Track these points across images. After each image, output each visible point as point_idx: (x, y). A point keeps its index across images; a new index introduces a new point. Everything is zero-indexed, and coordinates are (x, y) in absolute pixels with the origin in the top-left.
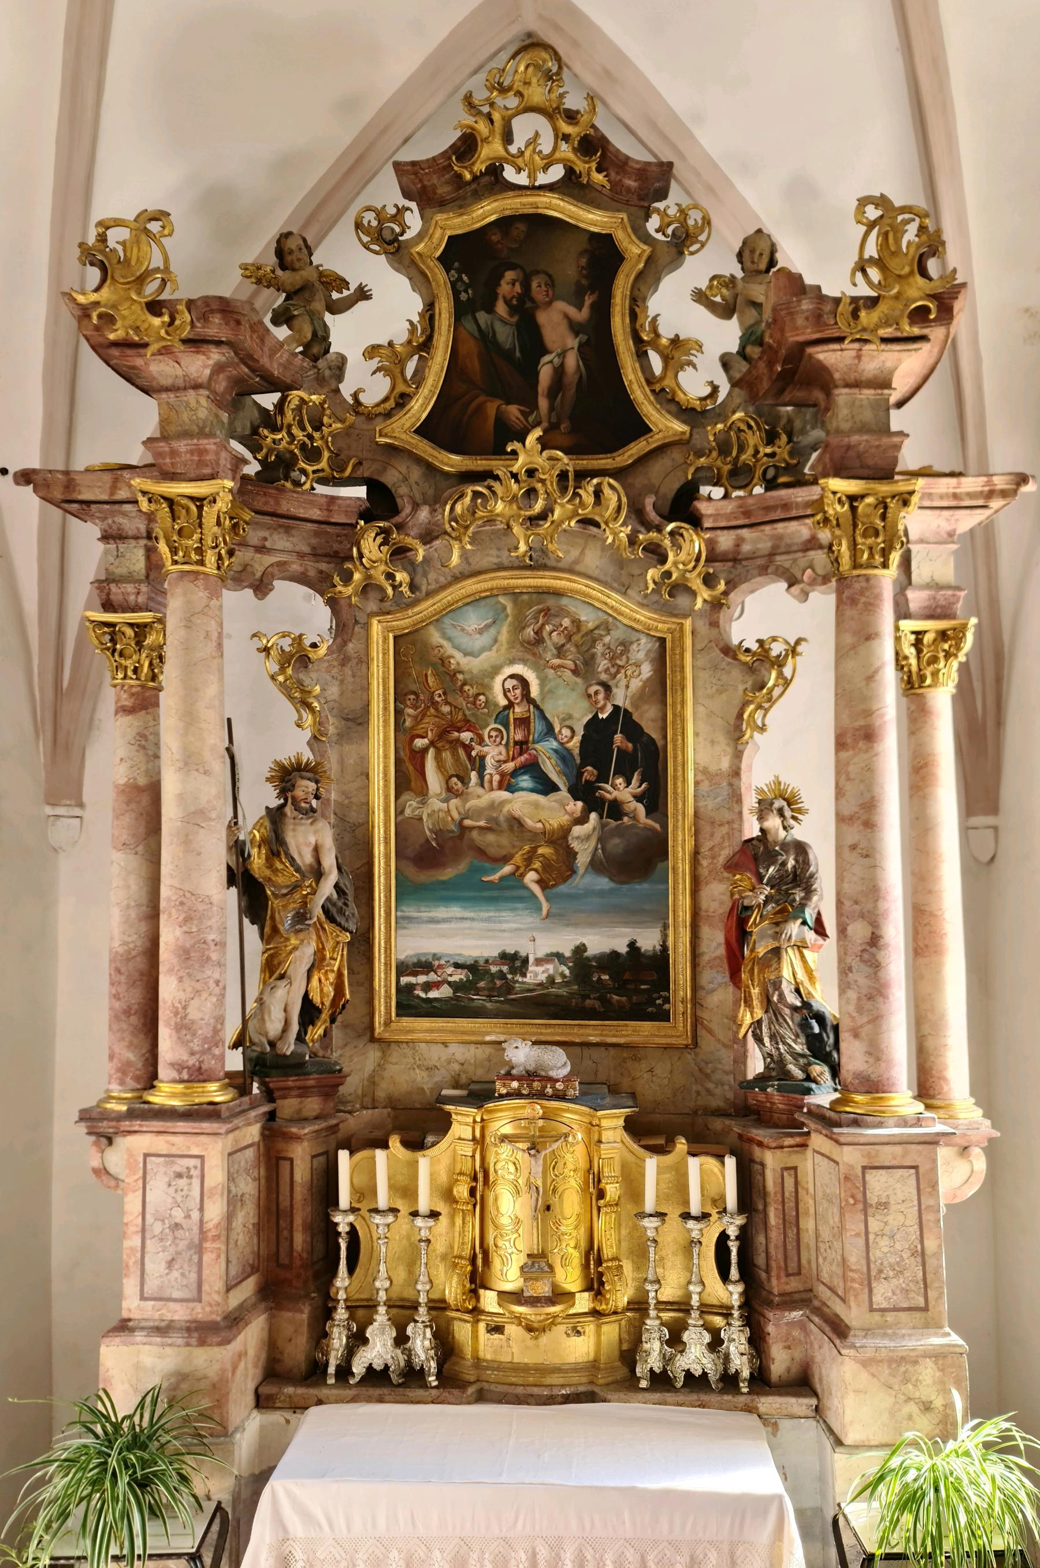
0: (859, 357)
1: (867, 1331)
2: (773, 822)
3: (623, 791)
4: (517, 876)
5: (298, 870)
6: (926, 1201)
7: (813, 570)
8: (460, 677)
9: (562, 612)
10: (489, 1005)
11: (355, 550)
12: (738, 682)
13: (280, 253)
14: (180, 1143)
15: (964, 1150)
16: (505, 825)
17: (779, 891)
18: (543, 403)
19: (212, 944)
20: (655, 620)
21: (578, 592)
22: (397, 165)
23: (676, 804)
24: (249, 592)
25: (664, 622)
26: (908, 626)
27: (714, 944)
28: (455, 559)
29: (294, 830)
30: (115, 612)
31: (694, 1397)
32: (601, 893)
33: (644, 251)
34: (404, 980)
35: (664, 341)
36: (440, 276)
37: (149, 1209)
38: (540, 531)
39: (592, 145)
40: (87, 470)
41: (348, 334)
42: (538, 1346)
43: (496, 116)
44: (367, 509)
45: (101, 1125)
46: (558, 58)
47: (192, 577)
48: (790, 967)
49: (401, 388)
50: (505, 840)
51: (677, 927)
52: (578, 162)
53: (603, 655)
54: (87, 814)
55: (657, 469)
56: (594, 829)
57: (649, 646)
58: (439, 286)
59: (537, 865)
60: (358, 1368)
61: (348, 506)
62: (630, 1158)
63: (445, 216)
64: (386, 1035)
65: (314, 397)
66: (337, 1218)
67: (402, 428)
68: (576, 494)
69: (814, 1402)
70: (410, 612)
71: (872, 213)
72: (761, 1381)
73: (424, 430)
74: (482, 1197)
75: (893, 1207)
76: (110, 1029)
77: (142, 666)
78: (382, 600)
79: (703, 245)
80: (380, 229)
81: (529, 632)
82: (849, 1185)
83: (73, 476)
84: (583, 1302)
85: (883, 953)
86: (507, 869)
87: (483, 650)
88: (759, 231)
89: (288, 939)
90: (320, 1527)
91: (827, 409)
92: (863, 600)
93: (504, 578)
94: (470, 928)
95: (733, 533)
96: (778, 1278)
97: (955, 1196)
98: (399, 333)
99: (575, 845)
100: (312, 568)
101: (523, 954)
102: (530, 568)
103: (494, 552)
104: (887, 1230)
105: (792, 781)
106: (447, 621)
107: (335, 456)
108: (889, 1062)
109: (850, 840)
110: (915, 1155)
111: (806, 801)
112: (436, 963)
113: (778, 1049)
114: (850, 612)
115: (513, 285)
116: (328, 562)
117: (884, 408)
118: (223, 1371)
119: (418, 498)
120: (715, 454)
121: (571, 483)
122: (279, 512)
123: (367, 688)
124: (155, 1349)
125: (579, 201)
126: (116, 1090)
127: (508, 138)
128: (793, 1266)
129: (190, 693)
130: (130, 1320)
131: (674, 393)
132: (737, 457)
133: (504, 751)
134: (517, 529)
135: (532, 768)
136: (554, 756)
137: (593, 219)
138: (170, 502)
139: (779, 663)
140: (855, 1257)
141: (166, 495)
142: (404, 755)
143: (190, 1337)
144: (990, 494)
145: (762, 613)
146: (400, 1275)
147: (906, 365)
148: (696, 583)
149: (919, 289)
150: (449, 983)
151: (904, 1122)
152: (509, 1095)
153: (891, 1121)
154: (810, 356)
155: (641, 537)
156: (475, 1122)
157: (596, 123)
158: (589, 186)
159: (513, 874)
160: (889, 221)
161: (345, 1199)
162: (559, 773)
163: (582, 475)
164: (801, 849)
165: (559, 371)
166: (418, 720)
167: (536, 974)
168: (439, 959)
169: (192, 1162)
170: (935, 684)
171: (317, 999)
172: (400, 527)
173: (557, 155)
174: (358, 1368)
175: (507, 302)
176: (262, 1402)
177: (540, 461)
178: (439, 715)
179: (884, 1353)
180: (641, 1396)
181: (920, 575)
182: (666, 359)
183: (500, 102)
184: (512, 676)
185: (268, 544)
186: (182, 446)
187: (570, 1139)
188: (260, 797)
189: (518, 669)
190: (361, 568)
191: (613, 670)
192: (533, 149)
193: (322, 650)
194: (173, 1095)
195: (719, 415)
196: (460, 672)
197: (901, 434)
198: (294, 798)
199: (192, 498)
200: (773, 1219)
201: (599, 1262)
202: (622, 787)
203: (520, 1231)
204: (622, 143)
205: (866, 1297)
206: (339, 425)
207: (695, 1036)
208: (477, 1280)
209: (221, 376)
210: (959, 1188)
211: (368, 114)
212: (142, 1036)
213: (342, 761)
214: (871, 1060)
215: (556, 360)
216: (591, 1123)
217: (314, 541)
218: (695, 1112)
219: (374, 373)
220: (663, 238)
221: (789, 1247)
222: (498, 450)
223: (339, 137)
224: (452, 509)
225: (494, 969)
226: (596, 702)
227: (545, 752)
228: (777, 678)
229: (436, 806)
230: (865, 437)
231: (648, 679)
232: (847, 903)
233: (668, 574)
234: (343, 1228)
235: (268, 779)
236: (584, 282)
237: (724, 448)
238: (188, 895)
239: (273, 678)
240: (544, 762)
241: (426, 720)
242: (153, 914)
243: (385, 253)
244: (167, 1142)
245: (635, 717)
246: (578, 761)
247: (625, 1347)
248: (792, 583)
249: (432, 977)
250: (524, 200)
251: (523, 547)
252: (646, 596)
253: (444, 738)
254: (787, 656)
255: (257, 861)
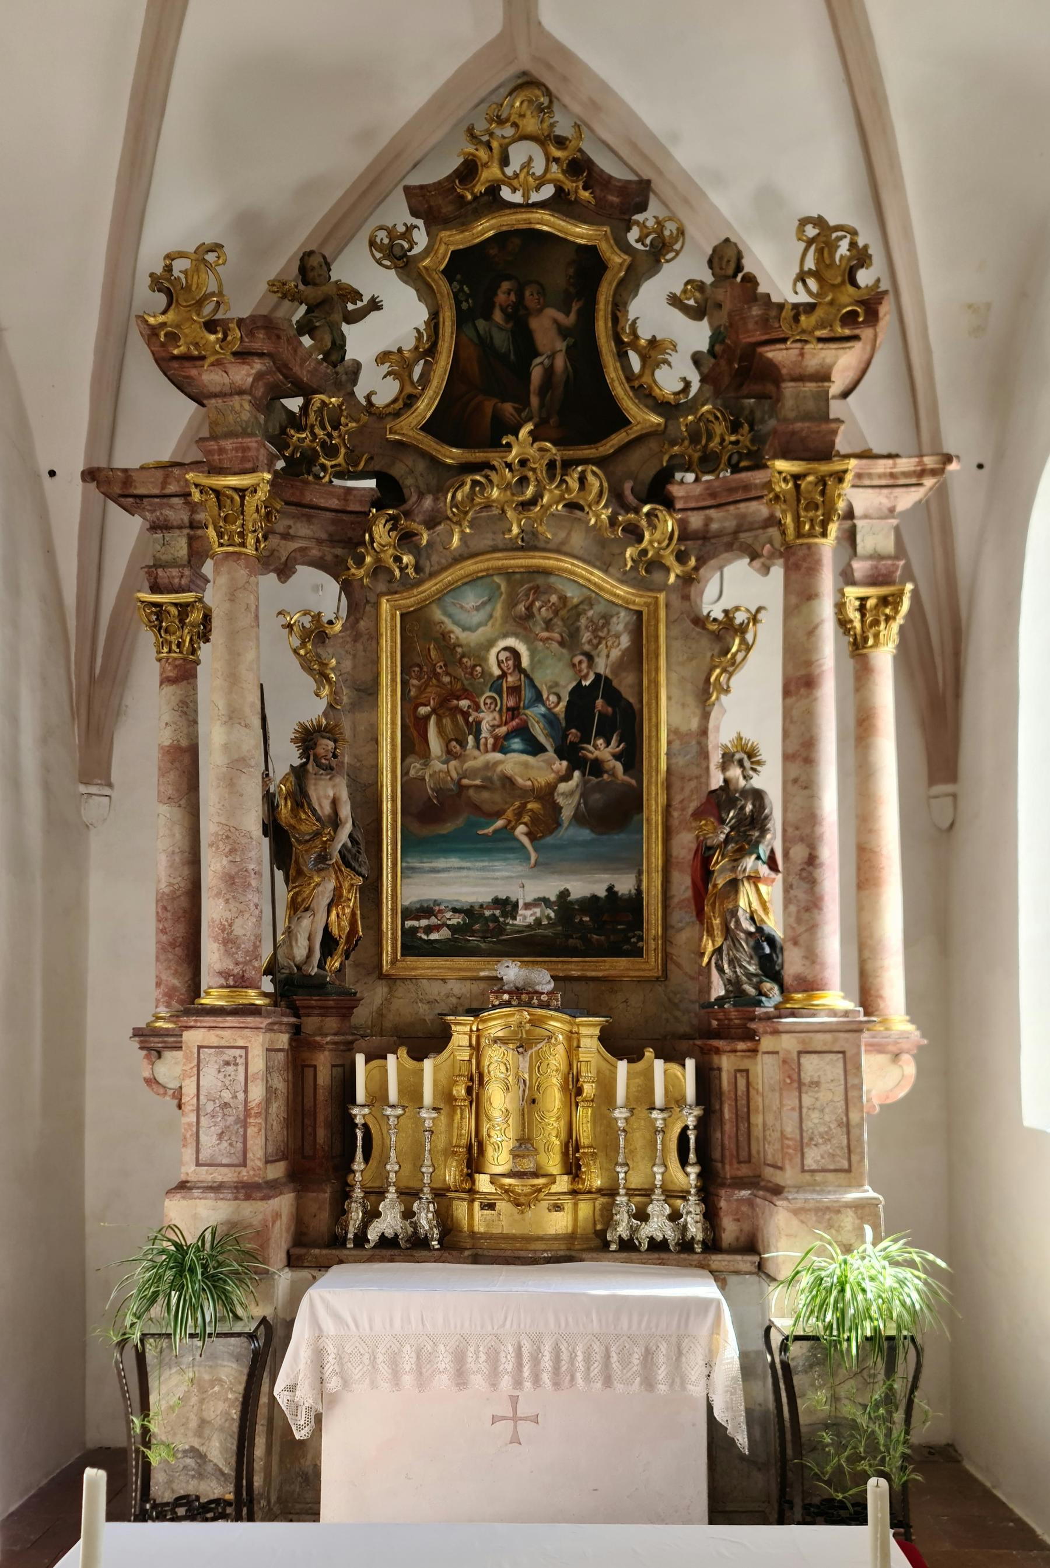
0: (802, 355)
1: (799, 1188)
2: (735, 772)
3: (602, 750)
4: (508, 830)
5: (319, 819)
6: (852, 1081)
7: (772, 545)
8: (459, 650)
9: (550, 589)
10: (483, 945)
11: (367, 535)
12: (706, 647)
13: (303, 270)
14: (227, 1037)
15: (896, 1056)
16: (498, 783)
17: (738, 832)
18: (534, 401)
19: (252, 873)
20: (633, 594)
21: (565, 570)
22: (407, 190)
23: (650, 762)
24: (273, 576)
25: (641, 596)
26: (852, 593)
27: (683, 887)
28: (456, 541)
29: (315, 784)
30: (161, 593)
31: (656, 1255)
32: (585, 844)
33: (625, 260)
34: (409, 924)
35: (643, 342)
36: (443, 287)
37: (203, 1092)
38: (531, 514)
39: (580, 167)
40: (142, 468)
41: (362, 342)
42: (524, 1220)
43: (495, 144)
44: (379, 499)
45: (153, 1042)
46: (548, 93)
47: (235, 558)
48: (746, 898)
49: (409, 389)
50: (497, 797)
51: (648, 877)
52: (567, 182)
53: (587, 627)
54: (114, 794)
55: (637, 456)
56: (577, 786)
57: (627, 619)
58: (443, 296)
59: (526, 819)
60: (373, 1235)
61: (362, 496)
62: (605, 1065)
63: (448, 233)
64: (393, 972)
65: (333, 400)
66: (355, 1111)
67: (408, 427)
68: (563, 481)
69: (756, 1259)
70: (415, 592)
71: (811, 231)
72: (713, 1245)
73: (429, 427)
74: (477, 1094)
75: (823, 1086)
76: (157, 959)
77: (184, 641)
78: (390, 582)
79: (678, 253)
80: (391, 246)
81: (521, 608)
82: (787, 1067)
83: (130, 473)
84: (563, 1184)
85: (818, 871)
86: (500, 823)
87: (479, 625)
88: (727, 240)
89: (311, 878)
90: (348, 1326)
91: (778, 400)
92: (805, 565)
93: (499, 559)
94: (466, 877)
95: (702, 513)
96: (731, 1164)
97: (887, 1097)
98: (409, 344)
99: (560, 800)
100: (330, 553)
101: (514, 899)
102: (522, 549)
103: (490, 535)
104: (818, 1105)
105: (750, 736)
106: (448, 600)
107: (350, 452)
108: (823, 965)
109: (793, 775)
110: (843, 1041)
111: (764, 754)
112: (437, 908)
113: (735, 972)
114: (794, 576)
115: (509, 294)
116: (340, 546)
117: (824, 398)
118: (265, 1220)
119: (423, 487)
120: (686, 443)
121: (558, 471)
122: (304, 502)
123: (377, 661)
124: (210, 1203)
125: (567, 216)
126: (163, 1011)
127: (505, 161)
128: (744, 1155)
129: (233, 656)
130: (188, 1182)
131: (651, 388)
132: (707, 445)
133: (497, 717)
134: (510, 514)
135: (523, 731)
136: (542, 720)
137: (581, 233)
138: (217, 493)
139: (742, 630)
140: (791, 1129)
141: (214, 487)
142: (409, 722)
143: (238, 1192)
144: (922, 473)
145: (737, 586)
146: (407, 1168)
147: (843, 362)
148: (670, 560)
149: (849, 296)
150: (448, 926)
151: (833, 1013)
152: (501, 1006)
153: (822, 1013)
154: (761, 355)
155: (620, 518)
156: (471, 1030)
157: (584, 148)
158: (577, 201)
159: (505, 827)
160: (824, 239)
161: (361, 1096)
162: (546, 736)
163: (568, 465)
164: (758, 796)
165: (549, 371)
166: (421, 690)
167: (526, 917)
168: (439, 905)
169: (238, 1052)
170: (876, 644)
171: (335, 931)
172: (408, 514)
173: (548, 176)
174: (373, 1235)
175: (503, 310)
176: (292, 1262)
177: (532, 452)
178: (441, 685)
179: (811, 1205)
180: (610, 1255)
181: (864, 547)
182: (644, 359)
183: (499, 132)
184: (505, 649)
185: (292, 532)
186: (228, 444)
187: (553, 1041)
188: (286, 755)
189: (511, 642)
190: (372, 552)
191: (595, 641)
192: (527, 170)
193: (338, 627)
194: (220, 998)
195: (691, 408)
196: (460, 646)
197: (838, 421)
198: (315, 756)
199: (236, 489)
200: (727, 1115)
201: (577, 1149)
202: (602, 748)
203: (510, 1122)
204: (605, 164)
205: (798, 1160)
206: (354, 425)
207: (665, 969)
208: (474, 1161)
209: (260, 383)
210: (891, 1090)
211: (383, 141)
212: (185, 965)
213: (354, 728)
214: (807, 963)
215: (546, 361)
216: (571, 1032)
217: (331, 528)
218: (665, 1037)
219: (385, 377)
220: (642, 248)
221: (741, 1139)
222: (495, 443)
223: (354, 163)
224: (454, 497)
225: (487, 913)
226: (580, 671)
227: (534, 715)
228: (740, 644)
229: (438, 766)
230: (807, 424)
231: (627, 649)
232: (790, 830)
233: (644, 552)
234: (359, 1120)
235: (292, 741)
236: (572, 290)
237: (694, 437)
238: (233, 830)
239: (295, 652)
240: (533, 726)
241: (429, 690)
242: (194, 861)
243: (396, 267)
244: (217, 1036)
245: (615, 683)
246: (564, 724)
247: (599, 1227)
248: (754, 556)
249: (433, 921)
250: (519, 216)
251: (515, 530)
252: (625, 573)
253: (445, 706)
254: (748, 623)
255: (285, 811)
